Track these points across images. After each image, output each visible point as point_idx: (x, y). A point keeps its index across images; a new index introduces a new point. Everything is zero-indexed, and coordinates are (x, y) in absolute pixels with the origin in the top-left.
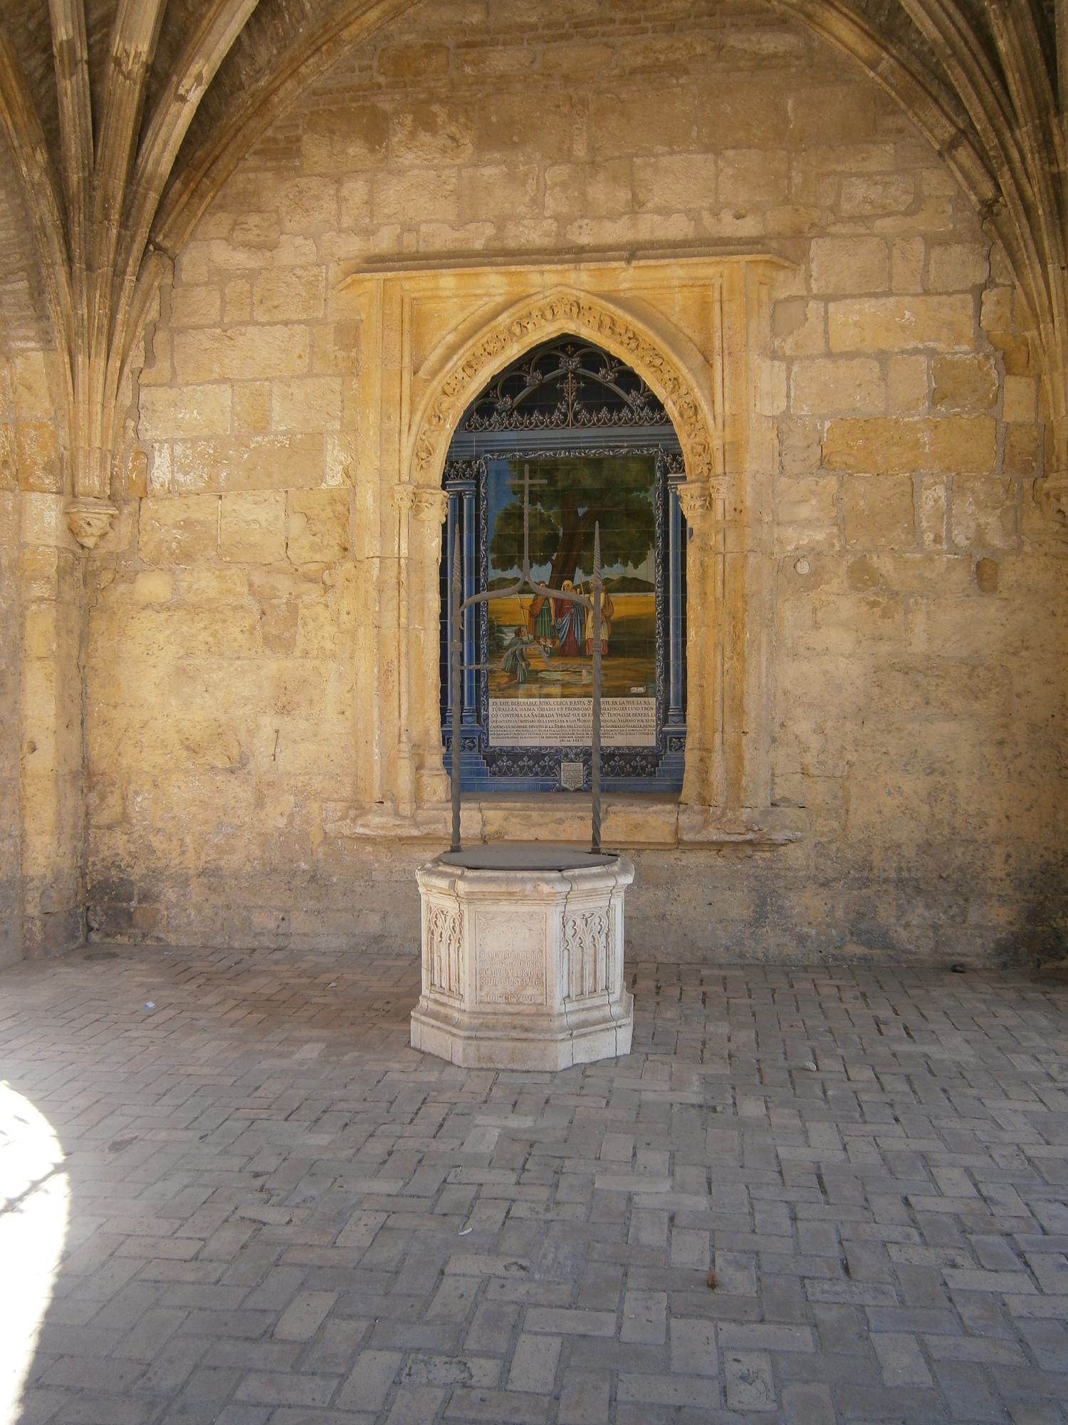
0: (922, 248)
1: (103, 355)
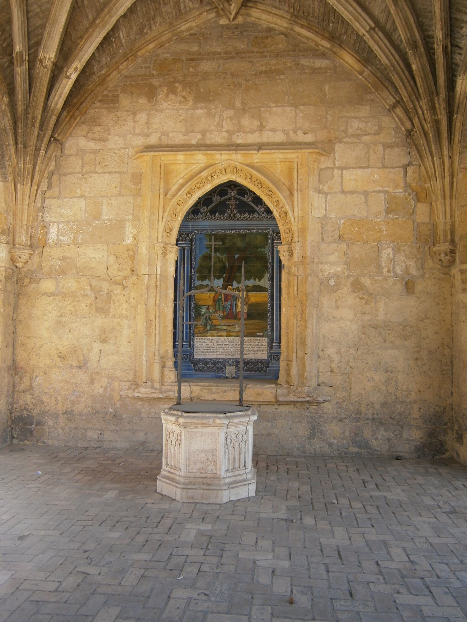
0: (382, 148)
1: (29, 185)
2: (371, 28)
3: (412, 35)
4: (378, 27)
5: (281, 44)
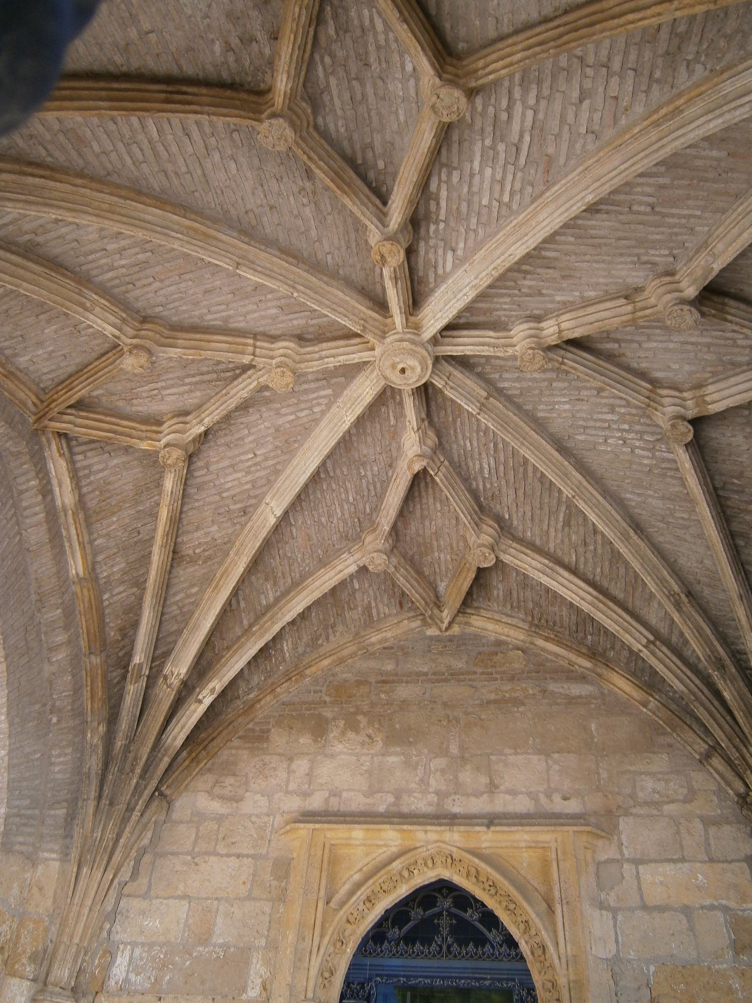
0: (701, 826)
1: (102, 869)
2: (649, 641)
3: (713, 650)
4: (660, 641)
5: (518, 662)
